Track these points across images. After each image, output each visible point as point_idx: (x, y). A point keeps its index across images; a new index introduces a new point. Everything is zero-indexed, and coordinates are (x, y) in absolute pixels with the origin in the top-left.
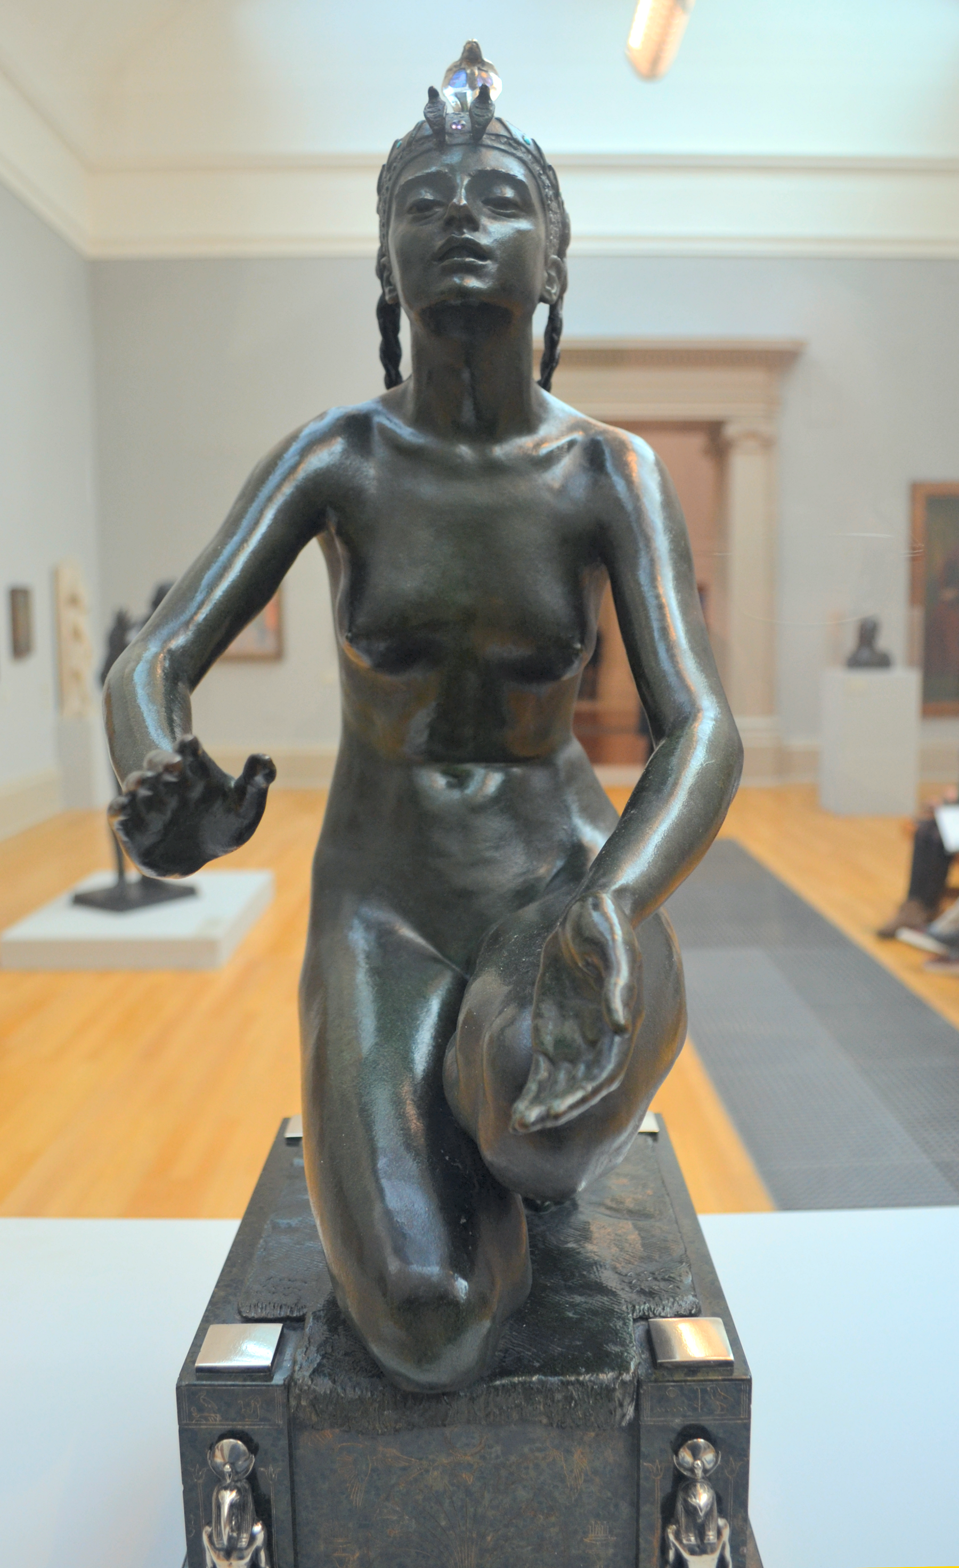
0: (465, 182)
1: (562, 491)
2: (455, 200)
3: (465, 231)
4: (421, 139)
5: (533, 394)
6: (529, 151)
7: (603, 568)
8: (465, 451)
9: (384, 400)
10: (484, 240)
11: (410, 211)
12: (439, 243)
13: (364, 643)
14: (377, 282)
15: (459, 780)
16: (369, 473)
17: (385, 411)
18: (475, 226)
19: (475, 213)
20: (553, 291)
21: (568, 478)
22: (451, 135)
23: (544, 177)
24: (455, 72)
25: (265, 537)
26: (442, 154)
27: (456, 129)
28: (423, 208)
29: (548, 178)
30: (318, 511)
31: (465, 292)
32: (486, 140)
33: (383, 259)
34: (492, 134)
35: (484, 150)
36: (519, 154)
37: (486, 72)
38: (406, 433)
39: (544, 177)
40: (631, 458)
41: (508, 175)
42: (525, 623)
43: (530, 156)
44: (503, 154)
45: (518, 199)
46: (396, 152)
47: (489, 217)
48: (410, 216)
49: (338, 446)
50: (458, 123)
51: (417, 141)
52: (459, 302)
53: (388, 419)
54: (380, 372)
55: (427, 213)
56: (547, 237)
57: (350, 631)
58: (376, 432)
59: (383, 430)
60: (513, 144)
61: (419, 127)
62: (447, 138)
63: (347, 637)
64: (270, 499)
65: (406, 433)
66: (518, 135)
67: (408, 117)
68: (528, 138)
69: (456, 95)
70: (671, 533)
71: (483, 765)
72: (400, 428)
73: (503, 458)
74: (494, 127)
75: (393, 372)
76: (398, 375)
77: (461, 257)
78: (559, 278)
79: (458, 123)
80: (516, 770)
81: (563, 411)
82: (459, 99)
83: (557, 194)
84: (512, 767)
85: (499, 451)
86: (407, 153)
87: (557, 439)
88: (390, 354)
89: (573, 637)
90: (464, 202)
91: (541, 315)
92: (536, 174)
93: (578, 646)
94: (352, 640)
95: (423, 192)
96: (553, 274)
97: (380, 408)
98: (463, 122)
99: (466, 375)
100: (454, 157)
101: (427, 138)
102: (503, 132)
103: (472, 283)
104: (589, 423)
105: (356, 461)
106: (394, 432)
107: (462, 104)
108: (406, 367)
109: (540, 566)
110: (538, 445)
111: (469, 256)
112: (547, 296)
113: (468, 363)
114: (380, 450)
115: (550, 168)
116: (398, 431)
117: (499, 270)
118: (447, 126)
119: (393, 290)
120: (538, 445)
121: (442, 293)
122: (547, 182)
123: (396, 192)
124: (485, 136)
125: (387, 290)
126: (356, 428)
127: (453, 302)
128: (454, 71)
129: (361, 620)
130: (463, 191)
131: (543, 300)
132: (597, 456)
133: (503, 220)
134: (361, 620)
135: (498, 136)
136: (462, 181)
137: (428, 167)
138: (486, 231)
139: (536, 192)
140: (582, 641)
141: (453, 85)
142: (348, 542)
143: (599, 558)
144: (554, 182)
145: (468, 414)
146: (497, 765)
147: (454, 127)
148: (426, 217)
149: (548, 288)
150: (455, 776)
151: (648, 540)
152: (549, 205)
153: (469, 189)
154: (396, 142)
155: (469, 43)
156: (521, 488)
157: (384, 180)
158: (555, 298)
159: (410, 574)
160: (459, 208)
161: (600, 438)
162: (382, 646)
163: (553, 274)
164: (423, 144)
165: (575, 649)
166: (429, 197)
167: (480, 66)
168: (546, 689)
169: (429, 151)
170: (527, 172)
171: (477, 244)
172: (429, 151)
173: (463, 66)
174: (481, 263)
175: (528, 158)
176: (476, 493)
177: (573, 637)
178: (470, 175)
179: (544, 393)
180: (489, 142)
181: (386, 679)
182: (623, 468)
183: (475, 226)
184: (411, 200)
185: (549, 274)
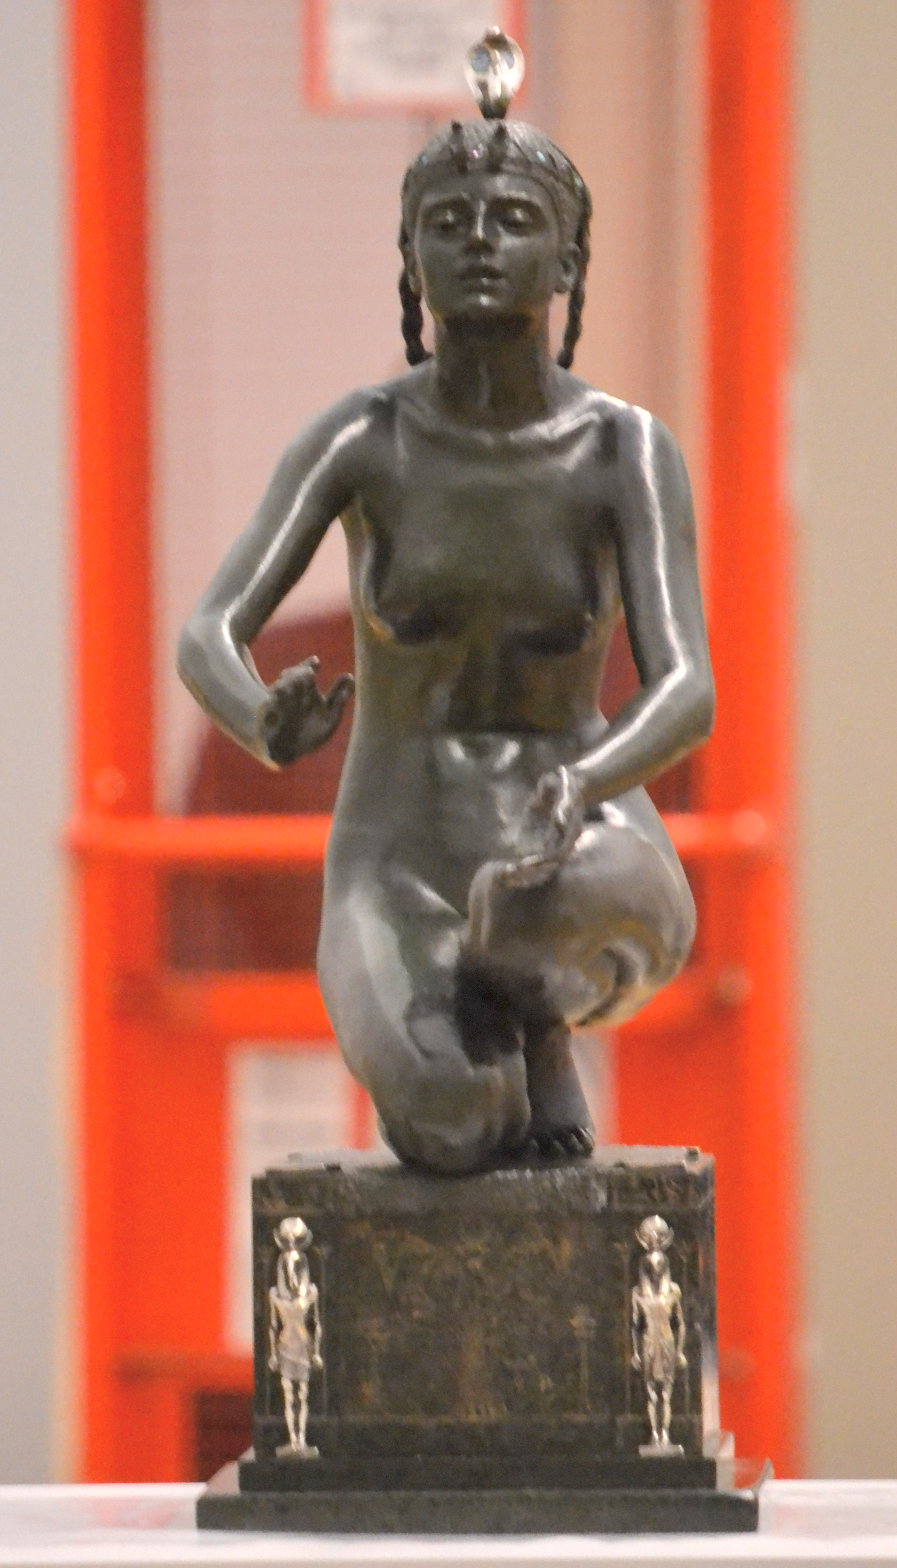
1: (575, 478)
8: (487, 438)
10: (497, 262)
15: (478, 751)
28: (446, 229)
31: (480, 308)
45: (531, 221)
54: (400, 344)
59: (407, 418)
88: (411, 327)
91: (559, 307)
93: (589, 617)
103: (485, 300)
126: (383, 410)
131: (559, 291)
134: (387, 593)
140: (594, 614)
153: (489, 216)
156: (533, 471)
175: (542, 176)
176: (494, 476)
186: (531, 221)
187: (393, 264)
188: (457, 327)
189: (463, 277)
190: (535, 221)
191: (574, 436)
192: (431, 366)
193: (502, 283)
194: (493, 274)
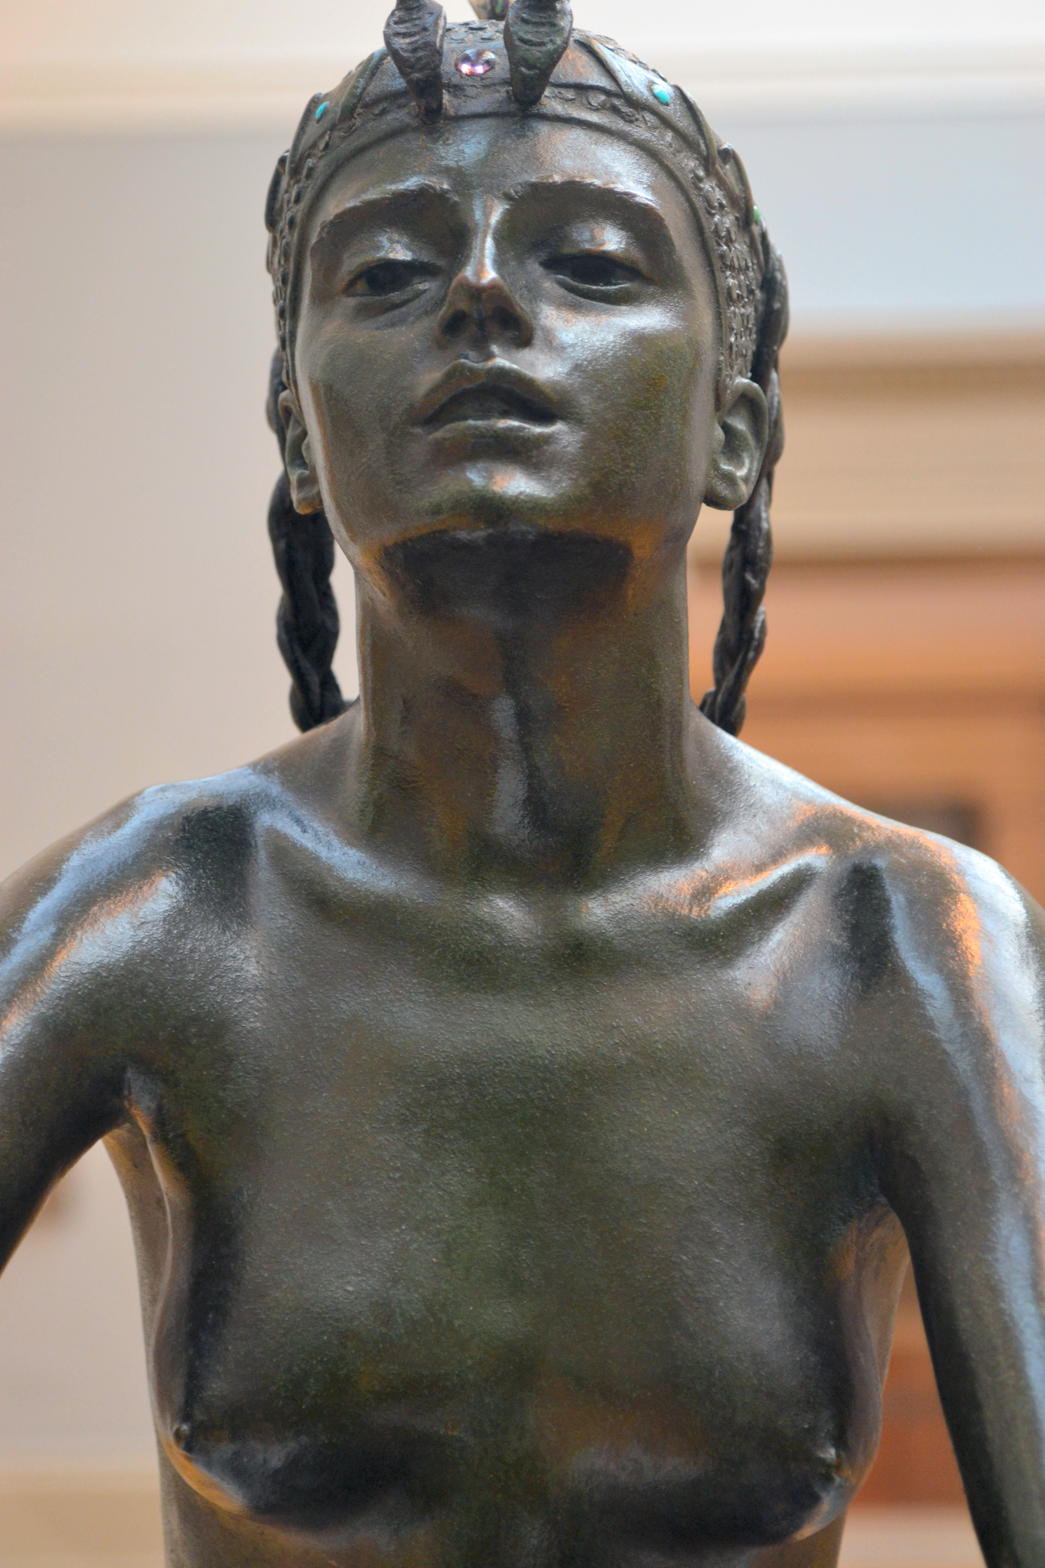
0: (495, 218)
3: (495, 349)
5: (690, 749)
6: (666, 123)
7: (894, 1219)
8: (507, 912)
9: (284, 766)
10: (543, 368)
11: (349, 289)
12: (428, 377)
13: (226, 1449)
14: (272, 440)
16: (247, 960)
17: (289, 798)
18: (520, 332)
19: (522, 304)
20: (741, 473)
21: (786, 981)
22: (457, 89)
23: (707, 186)
26: (435, 141)
27: (472, 75)
28: (384, 277)
29: (722, 184)
31: (493, 509)
32: (551, 102)
33: (284, 394)
34: (567, 86)
35: (544, 129)
36: (640, 132)
38: (350, 864)
40: (966, 921)
41: (611, 192)
43: (669, 136)
44: (595, 135)
45: (637, 255)
46: (313, 130)
48: (352, 302)
51: (366, 106)
52: (480, 534)
53: (298, 821)
55: (395, 296)
56: (720, 340)
57: (187, 1417)
58: (262, 856)
59: (284, 853)
61: (371, 68)
62: (446, 97)
63: (178, 1435)
65: (350, 864)
66: (634, 79)
68: (663, 89)
72: (329, 845)
73: (611, 930)
74: (575, 67)
75: (314, 680)
76: (329, 683)
77: (486, 415)
83: (747, 218)
85: (598, 911)
86: (345, 130)
87: (759, 868)
88: (305, 633)
89: (812, 1430)
90: (490, 275)
92: (687, 179)
93: (830, 1454)
96: (740, 425)
97: (275, 788)
98: (490, 56)
100: (468, 147)
101: (393, 97)
102: (596, 78)
103: (516, 484)
104: (848, 820)
105: (205, 939)
110: (705, 892)
111: (505, 414)
112: (723, 490)
113: (512, 685)
115: (728, 156)
116: (323, 853)
117: (588, 446)
118: (446, 67)
119: (309, 481)
120: (705, 892)
121: (436, 510)
122: (718, 195)
123: (314, 239)
124: (547, 92)
126: (212, 841)
127: (463, 535)
129: (218, 1387)
130: (489, 243)
131: (714, 501)
132: (869, 916)
133: (599, 312)
134: (218, 1387)
135: (582, 89)
136: (487, 215)
137: (396, 178)
140: (840, 1441)
142: (187, 1163)
143: (883, 1199)
144: (737, 190)
145: (507, 812)
147: (465, 68)
149: (725, 467)
153: (506, 237)
154: (315, 102)
156: (650, 1012)
157: (282, 195)
158: (745, 490)
160: (476, 293)
163: (740, 425)
164: (384, 112)
165: (823, 1462)
166: (401, 253)
170: (663, 178)
171: (526, 384)
174: (538, 430)
176: (536, 1028)
178: (508, 197)
179: (727, 739)
181: (289, 1540)
182: (944, 946)
183: (520, 332)
184: (352, 262)
185: (727, 429)
187: (260, 466)
191: (771, 906)
192: (354, 724)
193: (560, 432)
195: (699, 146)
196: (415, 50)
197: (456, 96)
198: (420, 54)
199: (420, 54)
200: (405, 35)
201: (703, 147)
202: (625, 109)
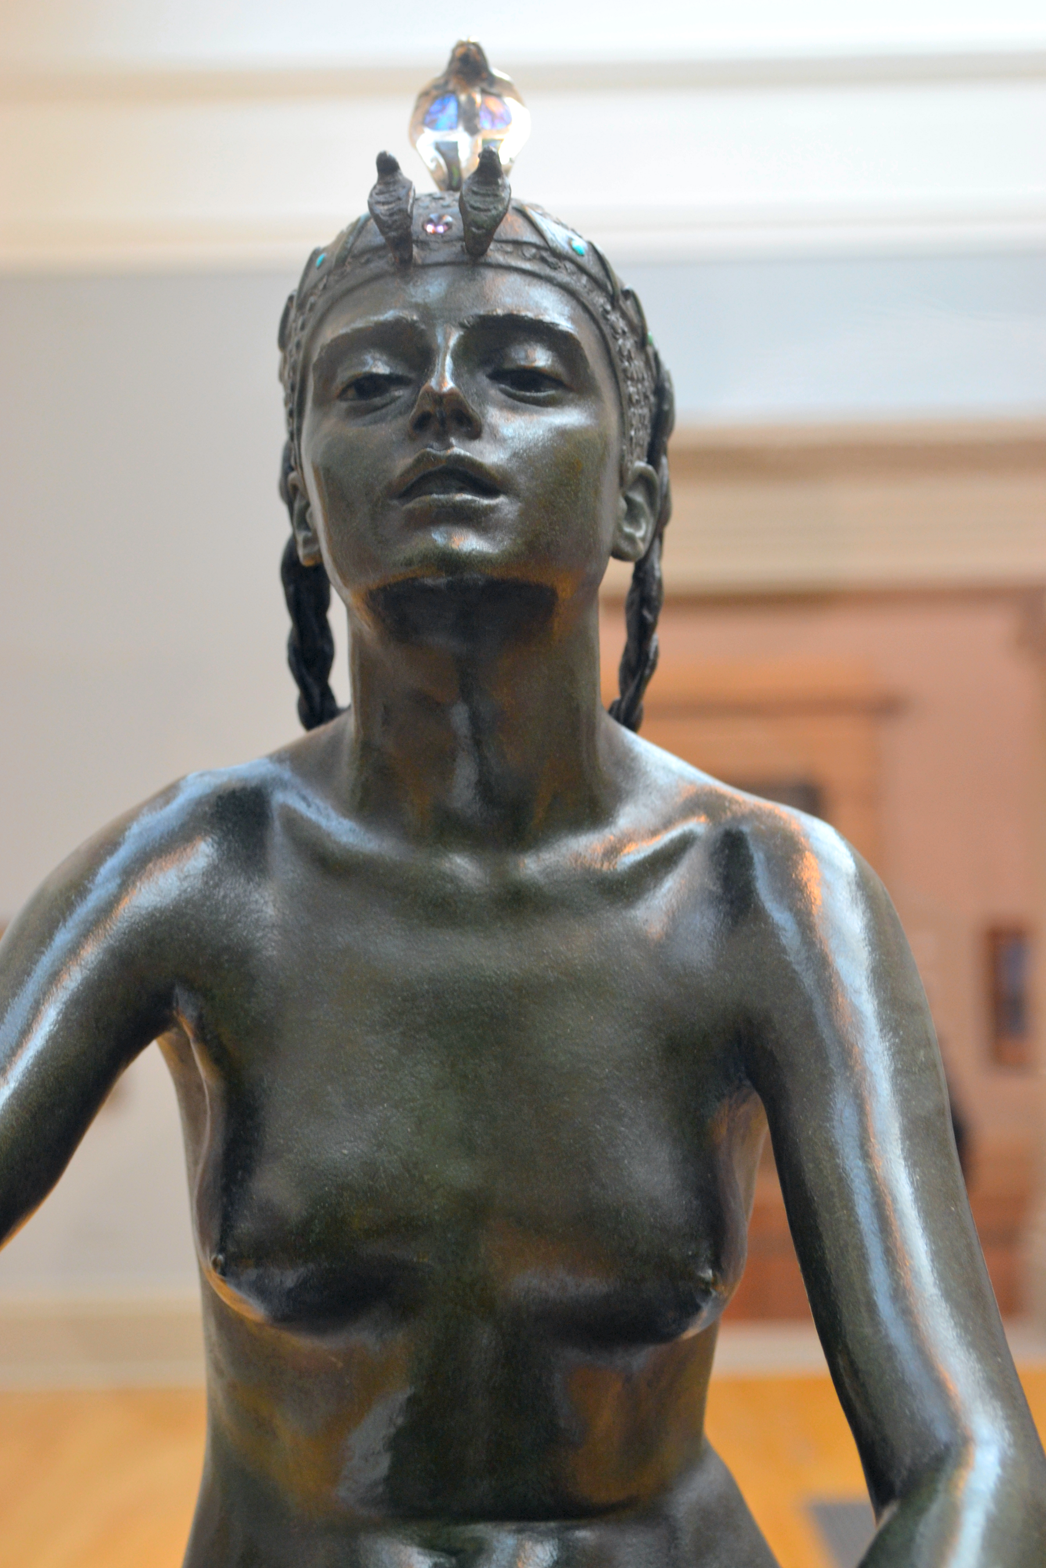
0: (453, 341)
2: (433, 383)
3: (453, 440)
4: (363, 253)
6: (582, 270)
7: (756, 1097)
8: (463, 867)
9: (295, 757)
10: (489, 455)
11: (342, 395)
12: (402, 462)
13: (251, 1274)
16: (266, 906)
17: (297, 781)
18: (472, 427)
19: (473, 407)
20: (639, 534)
21: (674, 918)
22: (424, 244)
23: (613, 317)
24: (436, 98)
25: (42, 1059)
26: (407, 283)
27: (435, 233)
28: (368, 387)
29: (624, 315)
30: (156, 990)
31: (452, 563)
32: (495, 254)
33: (293, 475)
34: (507, 242)
35: (489, 274)
36: (562, 277)
37: (498, 96)
38: (343, 831)
39: (613, 317)
40: (810, 872)
42: (594, 1227)
43: (584, 279)
44: (528, 279)
45: (560, 370)
46: (314, 275)
47: (502, 407)
48: (344, 405)
49: (202, 854)
50: (438, 217)
51: (354, 257)
52: (442, 581)
53: (304, 798)
54: (288, 692)
55: (377, 401)
56: (623, 433)
57: (222, 1250)
58: (277, 825)
59: (293, 822)
60: (549, 260)
61: (358, 228)
62: (415, 250)
63: (215, 1263)
64: (54, 977)
65: (343, 831)
66: (557, 236)
67: (344, 203)
68: (580, 244)
69: (438, 147)
70: (896, 1034)
71: (513, 1526)
73: (542, 880)
74: (513, 227)
75: (316, 691)
76: (327, 694)
77: (445, 491)
78: (652, 504)
79: (438, 217)
80: (585, 1535)
81: (668, 770)
82: (443, 154)
84: (578, 1528)
85: (531, 866)
87: (654, 833)
88: (309, 655)
89: (695, 1256)
90: (449, 385)
93: (709, 1274)
94: (226, 1269)
95: (368, 358)
96: (639, 497)
97: (287, 774)
99: (459, 716)
100: (432, 288)
102: (529, 236)
103: (469, 543)
104: (721, 797)
106: (319, 827)
107: (449, 164)
108: (341, 683)
109: (623, 1104)
110: (613, 852)
111: (461, 490)
112: (626, 547)
113: (466, 694)
114: (284, 862)
115: (629, 294)
116: (323, 822)
117: (523, 514)
118: (415, 228)
119: (311, 541)
120: (613, 852)
121: (409, 563)
122: (621, 324)
124: (492, 246)
125: (300, 538)
126: (239, 815)
127: (429, 582)
128: (433, 98)
130: (449, 361)
131: (619, 555)
133: (531, 413)
135: (518, 244)
136: (446, 340)
137: (377, 311)
138: (497, 439)
139: (602, 346)
140: (716, 1264)
141: (432, 124)
142: (222, 1059)
146: (542, 1526)
147: (430, 228)
148: (377, 408)
149: (628, 529)
150: (450, 1552)
151: (848, 1054)
152: (625, 371)
153: (463, 355)
154: (316, 254)
155: (461, 45)
156: (572, 943)
158: (642, 547)
159: (344, 1131)
160: (439, 398)
161: (746, 828)
162: (289, 1278)
163: (639, 497)
164: (368, 261)
165: (702, 1280)
166: (381, 368)
167: (485, 85)
168: (643, 1359)
169: (377, 277)
170: (580, 311)
172: (377, 277)
173: (451, 86)
174: (486, 502)
176: (484, 955)
177: (695, 1256)
178: (462, 326)
180: (500, 258)
181: (301, 1343)
182: (793, 890)
183: (472, 427)
184: (344, 375)
185: (629, 501)
186: (560, 370)
188: (396, 608)
189: (412, 487)
190: (566, 382)
191: (663, 861)
194: (483, 481)
195: (606, 286)
196: (391, 215)
197: (423, 249)
198: (396, 217)
199: (396, 217)
200: (384, 204)
201: (610, 288)
202: (551, 259)
